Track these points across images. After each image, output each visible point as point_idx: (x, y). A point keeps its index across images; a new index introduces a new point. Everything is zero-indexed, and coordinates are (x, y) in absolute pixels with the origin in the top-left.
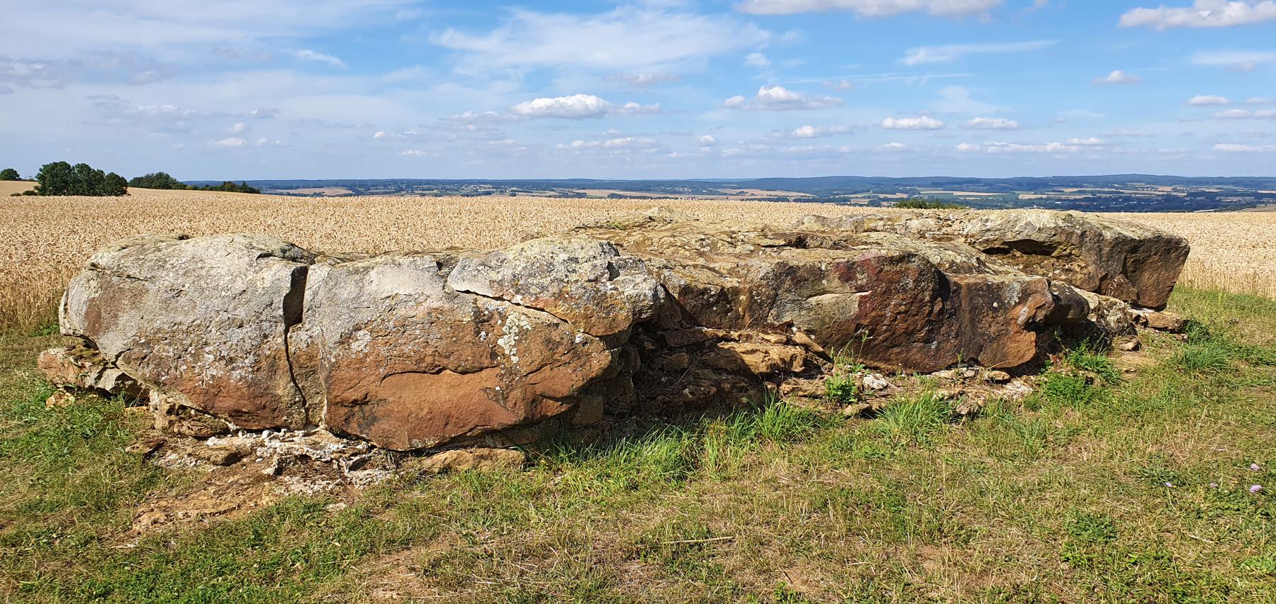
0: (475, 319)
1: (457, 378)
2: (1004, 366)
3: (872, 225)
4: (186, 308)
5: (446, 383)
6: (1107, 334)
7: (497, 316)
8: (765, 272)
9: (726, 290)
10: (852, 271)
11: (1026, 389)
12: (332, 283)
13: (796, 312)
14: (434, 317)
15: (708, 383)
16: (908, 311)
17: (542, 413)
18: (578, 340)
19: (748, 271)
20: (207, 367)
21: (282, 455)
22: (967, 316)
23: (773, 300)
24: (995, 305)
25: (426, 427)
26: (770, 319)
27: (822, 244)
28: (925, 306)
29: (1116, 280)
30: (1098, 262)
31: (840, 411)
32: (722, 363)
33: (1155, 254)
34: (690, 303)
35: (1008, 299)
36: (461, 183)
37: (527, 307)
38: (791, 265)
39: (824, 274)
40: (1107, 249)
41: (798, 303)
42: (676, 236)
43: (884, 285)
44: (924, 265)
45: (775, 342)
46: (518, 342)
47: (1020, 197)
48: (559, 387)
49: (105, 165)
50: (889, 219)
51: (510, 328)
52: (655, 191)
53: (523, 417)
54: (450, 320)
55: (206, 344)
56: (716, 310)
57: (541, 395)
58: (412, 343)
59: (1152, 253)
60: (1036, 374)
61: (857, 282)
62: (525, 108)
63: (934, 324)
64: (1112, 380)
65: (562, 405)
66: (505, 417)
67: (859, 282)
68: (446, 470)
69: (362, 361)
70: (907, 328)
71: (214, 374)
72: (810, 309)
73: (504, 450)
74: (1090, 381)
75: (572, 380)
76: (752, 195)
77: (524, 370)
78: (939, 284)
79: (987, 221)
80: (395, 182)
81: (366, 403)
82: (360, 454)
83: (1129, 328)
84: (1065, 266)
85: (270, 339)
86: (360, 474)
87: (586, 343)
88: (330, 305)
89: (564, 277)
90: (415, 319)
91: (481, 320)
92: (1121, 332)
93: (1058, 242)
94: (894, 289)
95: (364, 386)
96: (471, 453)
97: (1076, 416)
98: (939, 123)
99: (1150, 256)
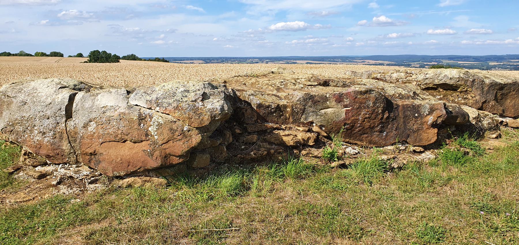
0: (139, 118)
1: (132, 145)
2: (421, 145)
3: (375, 76)
4: (27, 110)
5: (128, 147)
6: (482, 130)
7: (148, 117)
8: (299, 97)
9: (280, 106)
10: (342, 97)
11: (433, 157)
12: (83, 100)
13: (315, 117)
14: (121, 117)
15: (264, 149)
16: (370, 117)
17: (170, 162)
18: (185, 129)
19: (293, 97)
20: (35, 136)
21: (62, 176)
22: (402, 120)
23: (303, 111)
24: (416, 115)
25: (120, 167)
26: (302, 120)
27: (337, 84)
28: (379, 115)
29: (491, 104)
30: (481, 95)
31: (329, 164)
32: (273, 140)
33: (513, 91)
34: (262, 112)
35: (423, 112)
36: (231, 58)
37: (162, 113)
38: (312, 94)
39: (327, 99)
40: (487, 88)
41: (315, 113)
42: (270, 80)
43: (358, 105)
44: (378, 95)
45: (302, 131)
46: (158, 129)
47: (490, 64)
48: (176, 151)
49: (112, 52)
50: (383, 73)
51: (154, 123)
52: (325, 61)
53: (160, 164)
54: (128, 118)
55: (35, 126)
56: (275, 115)
57: (169, 154)
58: (113, 128)
59: (511, 91)
60: (437, 149)
61: (344, 103)
62: (273, 27)
63: (384, 124)
64: (479, 153)
65: (179, 159)
66: (154, 163)
67: (345, 103)
68: (130, 186)
69: (92, 136)
70: (370, 125)
71: (38, 139)
72: (321, 116)
73: (157, 178)
74: (467, 153)
75: (182, 148)
76: (368, 62)
77: (160, 142)
78: (387, 104)
79: (427, 74)
80: (221, 58)
81: (96, 154)
82: (95, 177)
83: (496, 127)
84: (464, 96)
85: (60, 125)
86: (92, 186)
87: (189, 131)
88: (82, 110)
89: (181, 99)
90: (113, 117)
91: (142, 118)
92: (490, 129)
93: (460, 85)
94: (363, 106)
95: (94, 147)
96: (141, 179)
97: (455, 170)
98: (455, 31)
99: (510, 92)
